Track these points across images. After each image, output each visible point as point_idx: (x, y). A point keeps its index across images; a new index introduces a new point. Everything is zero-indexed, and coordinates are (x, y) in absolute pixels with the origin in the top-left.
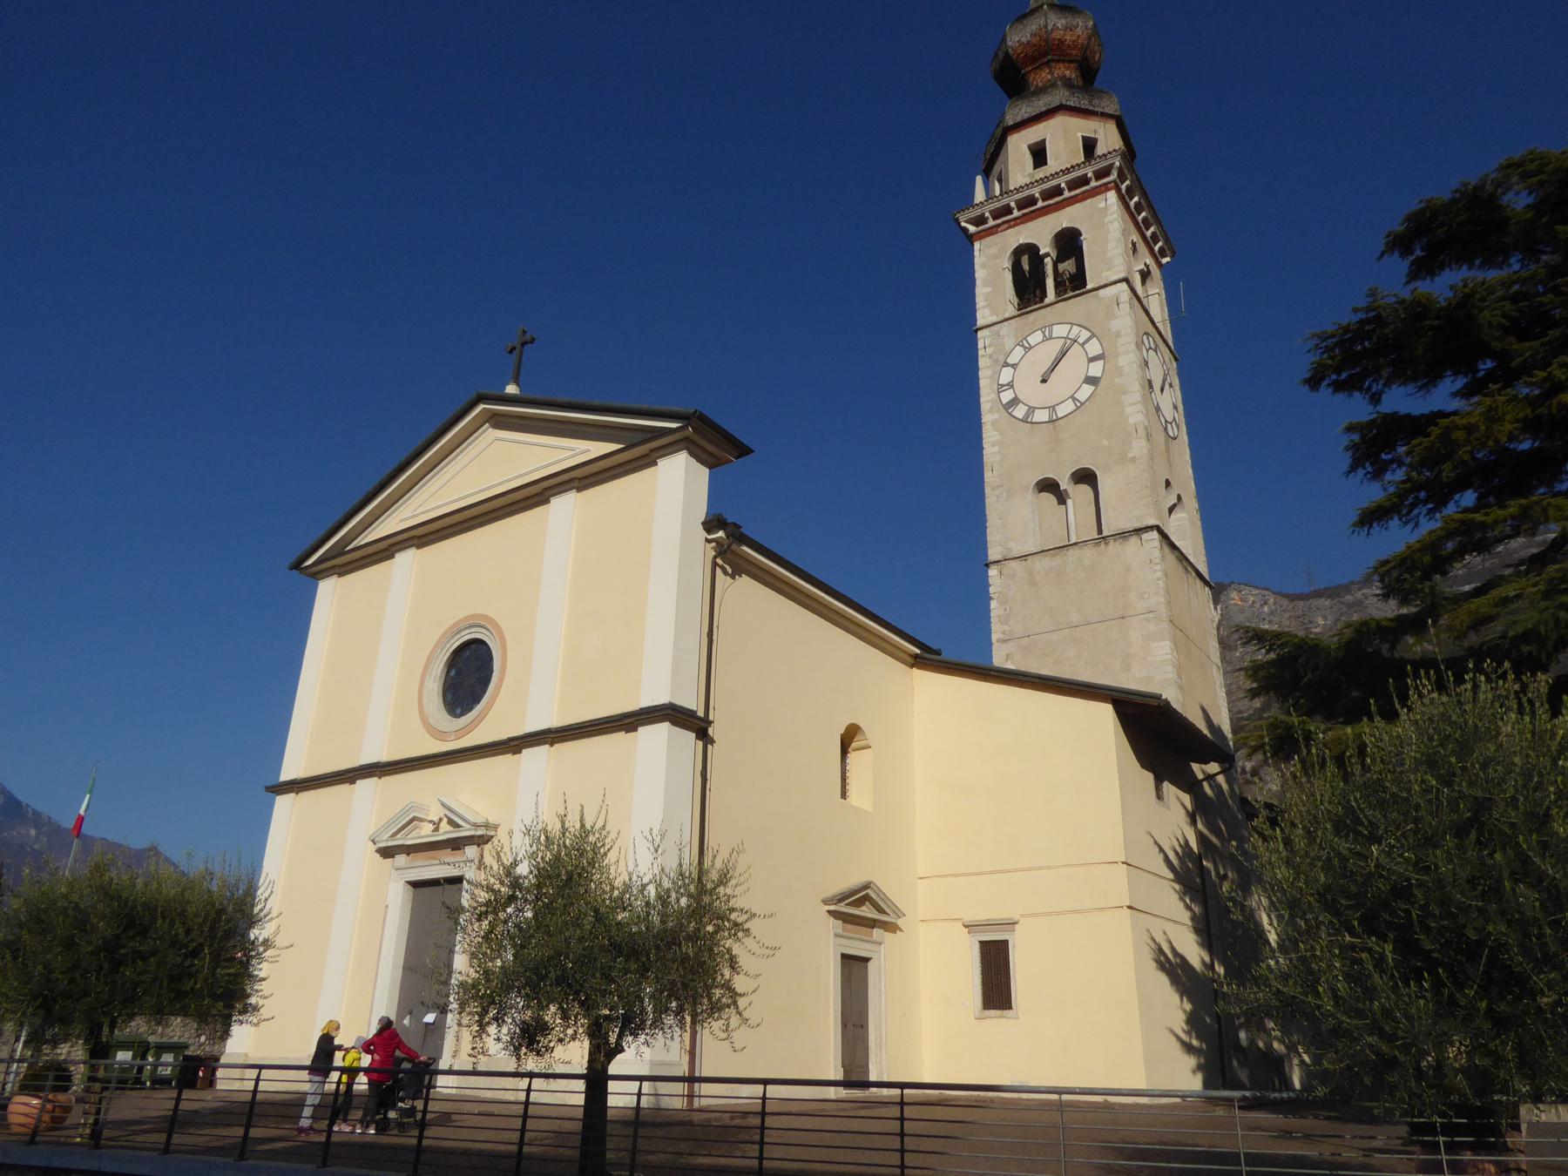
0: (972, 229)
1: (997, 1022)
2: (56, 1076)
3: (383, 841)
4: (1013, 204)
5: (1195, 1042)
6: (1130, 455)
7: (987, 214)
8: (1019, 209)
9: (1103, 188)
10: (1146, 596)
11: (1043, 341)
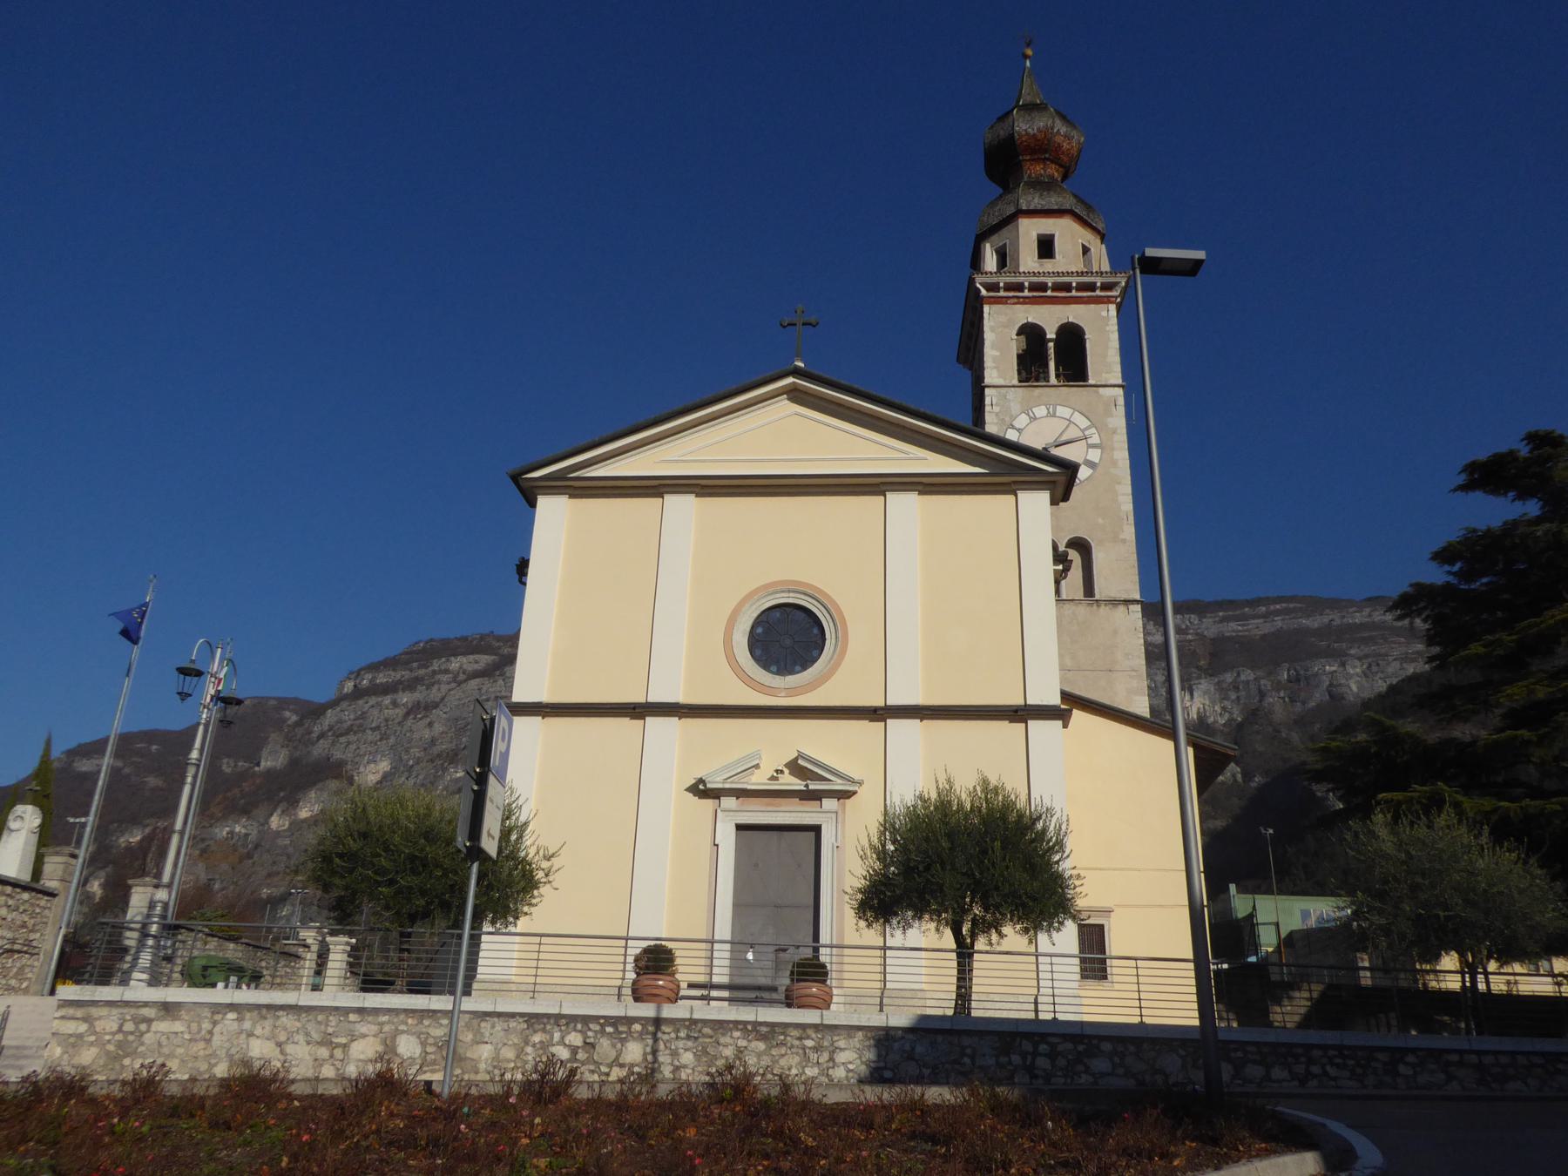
0: (984, 292)
2: (407, 982)
6: (1122, 537)
10: (1130, 657)
11: (1047, 416)
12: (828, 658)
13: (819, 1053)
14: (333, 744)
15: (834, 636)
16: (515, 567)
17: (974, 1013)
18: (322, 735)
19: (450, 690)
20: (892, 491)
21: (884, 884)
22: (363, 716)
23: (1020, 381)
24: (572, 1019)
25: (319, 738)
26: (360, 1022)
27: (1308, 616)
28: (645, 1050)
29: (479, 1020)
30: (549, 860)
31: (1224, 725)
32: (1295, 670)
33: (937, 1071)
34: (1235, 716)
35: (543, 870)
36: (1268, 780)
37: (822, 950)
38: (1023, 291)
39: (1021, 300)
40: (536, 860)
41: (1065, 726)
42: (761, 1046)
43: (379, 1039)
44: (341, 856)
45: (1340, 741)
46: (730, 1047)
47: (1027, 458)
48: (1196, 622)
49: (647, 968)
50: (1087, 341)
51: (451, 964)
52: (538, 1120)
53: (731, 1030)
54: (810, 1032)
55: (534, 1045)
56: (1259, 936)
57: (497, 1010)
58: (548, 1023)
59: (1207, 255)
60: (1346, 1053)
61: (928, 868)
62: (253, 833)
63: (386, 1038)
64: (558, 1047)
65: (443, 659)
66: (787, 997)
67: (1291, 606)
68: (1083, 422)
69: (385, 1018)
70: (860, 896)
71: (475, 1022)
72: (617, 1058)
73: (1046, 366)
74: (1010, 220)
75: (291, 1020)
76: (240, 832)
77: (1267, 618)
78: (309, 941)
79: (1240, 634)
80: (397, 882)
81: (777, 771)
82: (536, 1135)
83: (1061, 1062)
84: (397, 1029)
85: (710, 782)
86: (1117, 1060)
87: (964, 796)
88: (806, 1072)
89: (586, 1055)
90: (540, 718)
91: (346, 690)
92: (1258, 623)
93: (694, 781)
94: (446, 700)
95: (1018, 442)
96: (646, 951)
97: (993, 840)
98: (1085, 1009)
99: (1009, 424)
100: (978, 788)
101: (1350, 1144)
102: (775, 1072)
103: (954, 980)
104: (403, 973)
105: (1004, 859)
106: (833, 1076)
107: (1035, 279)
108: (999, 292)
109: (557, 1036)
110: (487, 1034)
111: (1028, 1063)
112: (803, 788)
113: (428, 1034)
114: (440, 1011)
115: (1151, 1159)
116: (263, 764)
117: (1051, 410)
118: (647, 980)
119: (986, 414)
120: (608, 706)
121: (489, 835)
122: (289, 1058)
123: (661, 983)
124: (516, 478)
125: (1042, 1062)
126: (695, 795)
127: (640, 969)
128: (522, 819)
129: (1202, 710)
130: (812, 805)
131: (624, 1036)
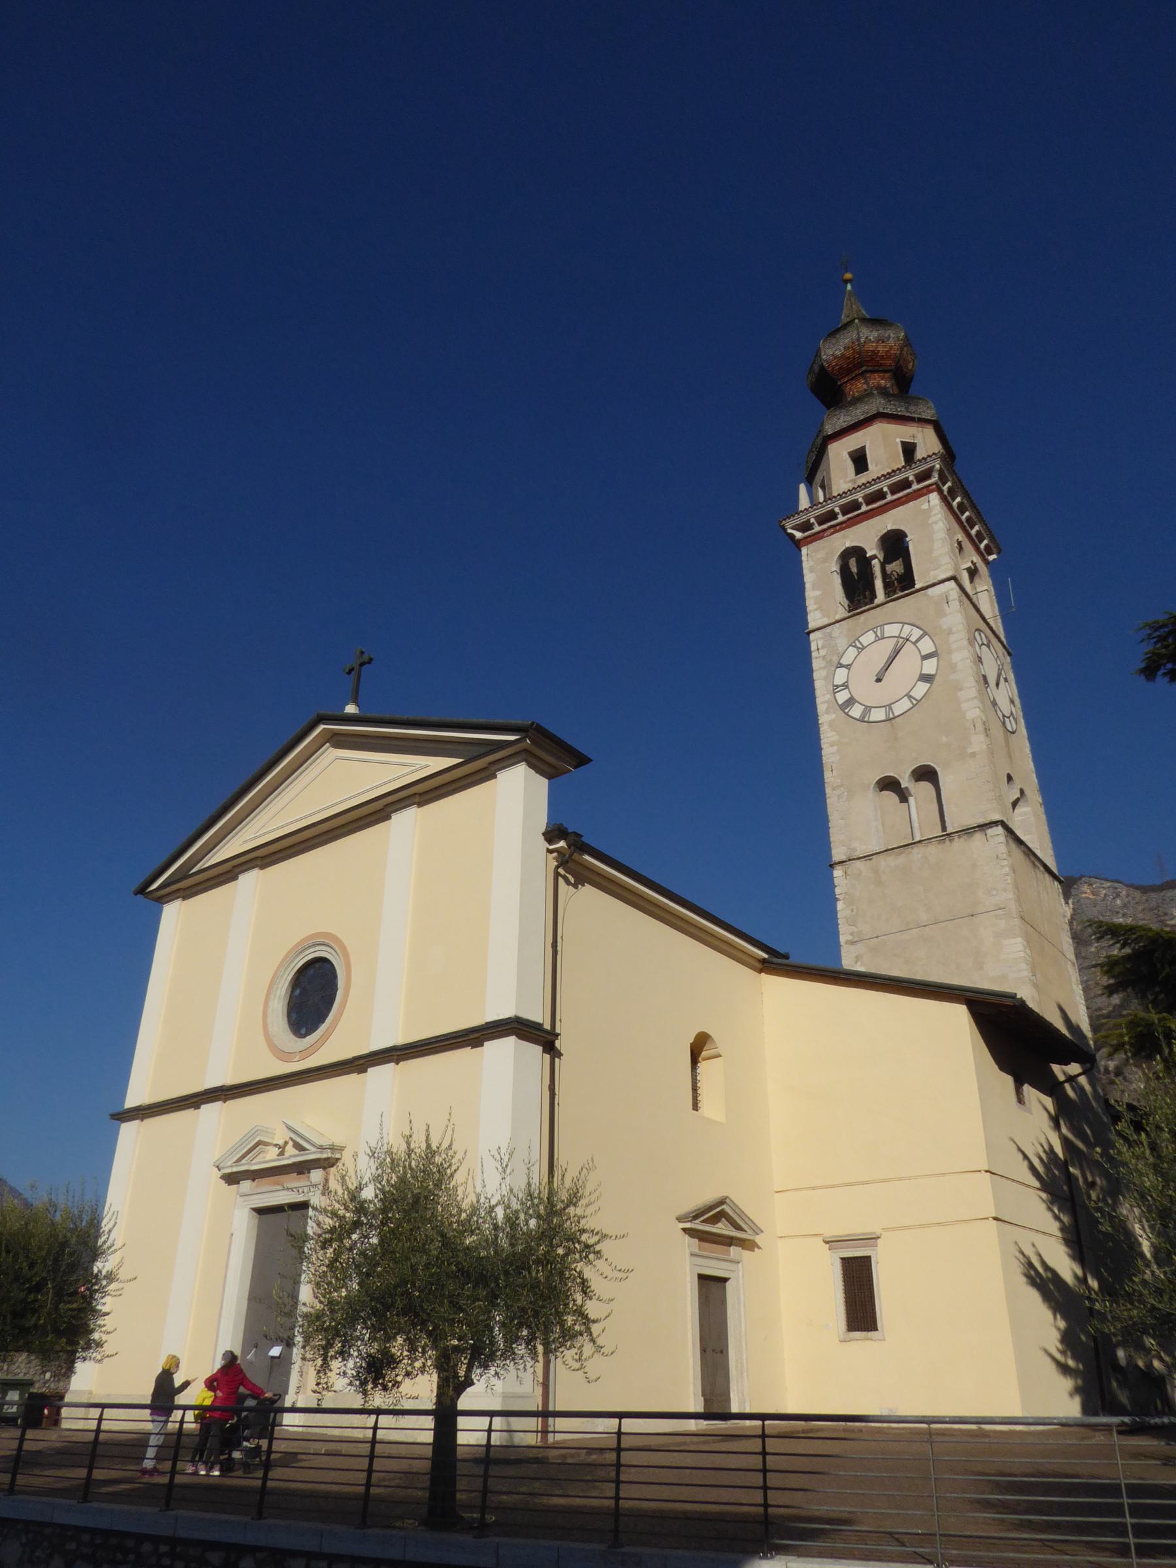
0: (798, 535)
1: (862, 1345)
4: (837, 510)
5: (1071, 1363)
6: (970, 750)
7: (812, 520)
8: (844, 514)
9: (925, 491)
20: (397, 810)
38: (836, 518)
50: (910, 543)
99: (836, 662)
107: (868, 491)
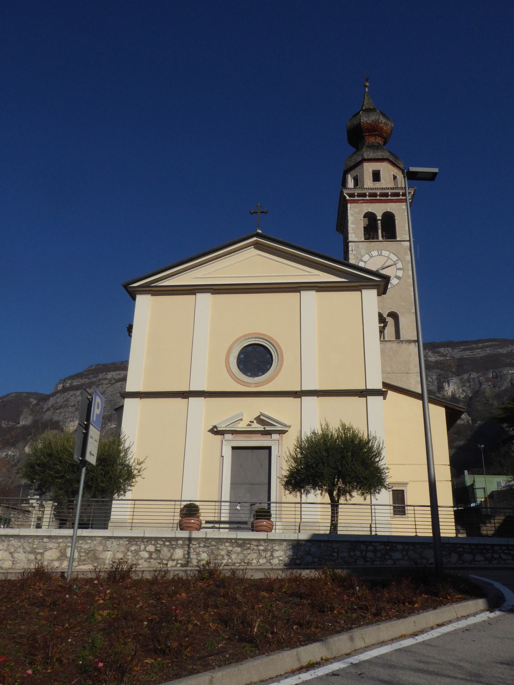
0: (348, 198)
3: (222, 427)
12: (274, 369)
13: (266, 552)
14: (54, 413)
15: (277, 358)
16: (127, 329)
17: (339, 533)
18: (48, 410)
19: (108, 387)
21: (297, 474)
22: (67, 400)
23: (365, 239)
24: (150, 539)
25: (47, 410)
26: (49, 542)
27: (501, 348)
28: (184, 552)
29: (106, 540)
30: (140, 465)
31: (463, 398)
32: (496, 373)
33: (321, 559)
34: (468, 394)
35: (137, 469)
36: (483, 423)
37: (272, 505)
38: (366, 197)
39: (365, 201)
40: (133, 465)
41: (385, 399)
42: (239, 549)
43: (58, 550)
44: (39, 465)
45: (512, 404)
46: (224, 550)
47: (373, 277)
48: (450, 351)
49: (186, 514)
50: (396, 220)
51: (92, 515)
52: (108, 591)
53: (225, 543)
54: (262, 543)
55: (132, 551)
56: (476, 494)
57: (114, 536)
58: (139, 541)
59: (439, 170)
60: (510, 548)
61: (317, 465)
62: (17, 455)
63: (61, 550)
64: (143, 552)
65: (104, 373)
66: (252, 527)
67: (494, 343)
68: (394, 258)
69: (61, 540)
70: (286, 479)
71: (104, 541)
72: (171, 556)
73: (377, 232)
74: (360, 163)
75: (16, 542)
76: (11, 454)
77: (483, 349)
78: (35, 505)
79: (470, 356)
80: (65, 477)
81: (250, 422)
82: (107, 598)
83: (379, 554)
84: (66, 545)
85: (219, 427)
86: (405, 553)
87: (334, 432)
88: (260, 561)
89: (157, 556)
90: (139, 399)
91: (59, 388)
92: (479, 352)
93: (212, 427)
94: (106, 392)
95: (364, 268)
96: (185, 506)
97: (347, 452)
98: (393, 530)
100: (340, 428)
101: (503, 594)
102: (245, 562)
103: (330, 517)
104: (70, 519)
105: (352, 461)
106: (273, 563)
108: (355, 197)
109: (142, 547)
110: (109, 547)
111: (363, 555)
112: (263, 429)
113: (81, 547)
114: (87, 537)
115: (404, 604)
116: (21, 423)
117: (380, 253)
118: (186, 520)
119: (350, 255)
120: (176, 393)
121: (91, 454)
122: (16, 559)
123: (192, 521)
124: (126, 287)
125: (370, 555)
126: (212, 434)
127: (183, 515)
128: (127, 446)
129: (453, 391)
130: (268, 437)
131: (174, 546)
